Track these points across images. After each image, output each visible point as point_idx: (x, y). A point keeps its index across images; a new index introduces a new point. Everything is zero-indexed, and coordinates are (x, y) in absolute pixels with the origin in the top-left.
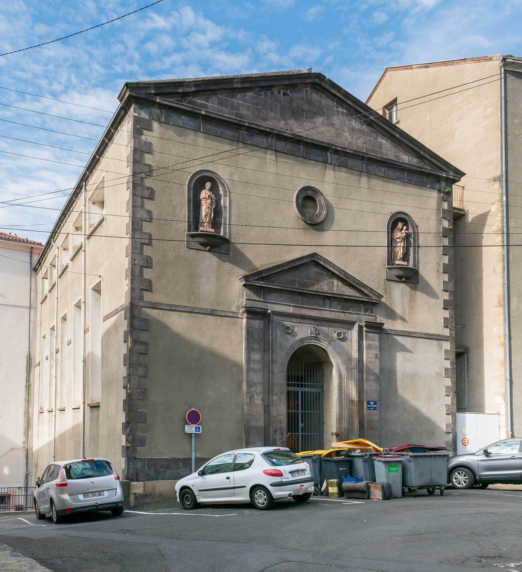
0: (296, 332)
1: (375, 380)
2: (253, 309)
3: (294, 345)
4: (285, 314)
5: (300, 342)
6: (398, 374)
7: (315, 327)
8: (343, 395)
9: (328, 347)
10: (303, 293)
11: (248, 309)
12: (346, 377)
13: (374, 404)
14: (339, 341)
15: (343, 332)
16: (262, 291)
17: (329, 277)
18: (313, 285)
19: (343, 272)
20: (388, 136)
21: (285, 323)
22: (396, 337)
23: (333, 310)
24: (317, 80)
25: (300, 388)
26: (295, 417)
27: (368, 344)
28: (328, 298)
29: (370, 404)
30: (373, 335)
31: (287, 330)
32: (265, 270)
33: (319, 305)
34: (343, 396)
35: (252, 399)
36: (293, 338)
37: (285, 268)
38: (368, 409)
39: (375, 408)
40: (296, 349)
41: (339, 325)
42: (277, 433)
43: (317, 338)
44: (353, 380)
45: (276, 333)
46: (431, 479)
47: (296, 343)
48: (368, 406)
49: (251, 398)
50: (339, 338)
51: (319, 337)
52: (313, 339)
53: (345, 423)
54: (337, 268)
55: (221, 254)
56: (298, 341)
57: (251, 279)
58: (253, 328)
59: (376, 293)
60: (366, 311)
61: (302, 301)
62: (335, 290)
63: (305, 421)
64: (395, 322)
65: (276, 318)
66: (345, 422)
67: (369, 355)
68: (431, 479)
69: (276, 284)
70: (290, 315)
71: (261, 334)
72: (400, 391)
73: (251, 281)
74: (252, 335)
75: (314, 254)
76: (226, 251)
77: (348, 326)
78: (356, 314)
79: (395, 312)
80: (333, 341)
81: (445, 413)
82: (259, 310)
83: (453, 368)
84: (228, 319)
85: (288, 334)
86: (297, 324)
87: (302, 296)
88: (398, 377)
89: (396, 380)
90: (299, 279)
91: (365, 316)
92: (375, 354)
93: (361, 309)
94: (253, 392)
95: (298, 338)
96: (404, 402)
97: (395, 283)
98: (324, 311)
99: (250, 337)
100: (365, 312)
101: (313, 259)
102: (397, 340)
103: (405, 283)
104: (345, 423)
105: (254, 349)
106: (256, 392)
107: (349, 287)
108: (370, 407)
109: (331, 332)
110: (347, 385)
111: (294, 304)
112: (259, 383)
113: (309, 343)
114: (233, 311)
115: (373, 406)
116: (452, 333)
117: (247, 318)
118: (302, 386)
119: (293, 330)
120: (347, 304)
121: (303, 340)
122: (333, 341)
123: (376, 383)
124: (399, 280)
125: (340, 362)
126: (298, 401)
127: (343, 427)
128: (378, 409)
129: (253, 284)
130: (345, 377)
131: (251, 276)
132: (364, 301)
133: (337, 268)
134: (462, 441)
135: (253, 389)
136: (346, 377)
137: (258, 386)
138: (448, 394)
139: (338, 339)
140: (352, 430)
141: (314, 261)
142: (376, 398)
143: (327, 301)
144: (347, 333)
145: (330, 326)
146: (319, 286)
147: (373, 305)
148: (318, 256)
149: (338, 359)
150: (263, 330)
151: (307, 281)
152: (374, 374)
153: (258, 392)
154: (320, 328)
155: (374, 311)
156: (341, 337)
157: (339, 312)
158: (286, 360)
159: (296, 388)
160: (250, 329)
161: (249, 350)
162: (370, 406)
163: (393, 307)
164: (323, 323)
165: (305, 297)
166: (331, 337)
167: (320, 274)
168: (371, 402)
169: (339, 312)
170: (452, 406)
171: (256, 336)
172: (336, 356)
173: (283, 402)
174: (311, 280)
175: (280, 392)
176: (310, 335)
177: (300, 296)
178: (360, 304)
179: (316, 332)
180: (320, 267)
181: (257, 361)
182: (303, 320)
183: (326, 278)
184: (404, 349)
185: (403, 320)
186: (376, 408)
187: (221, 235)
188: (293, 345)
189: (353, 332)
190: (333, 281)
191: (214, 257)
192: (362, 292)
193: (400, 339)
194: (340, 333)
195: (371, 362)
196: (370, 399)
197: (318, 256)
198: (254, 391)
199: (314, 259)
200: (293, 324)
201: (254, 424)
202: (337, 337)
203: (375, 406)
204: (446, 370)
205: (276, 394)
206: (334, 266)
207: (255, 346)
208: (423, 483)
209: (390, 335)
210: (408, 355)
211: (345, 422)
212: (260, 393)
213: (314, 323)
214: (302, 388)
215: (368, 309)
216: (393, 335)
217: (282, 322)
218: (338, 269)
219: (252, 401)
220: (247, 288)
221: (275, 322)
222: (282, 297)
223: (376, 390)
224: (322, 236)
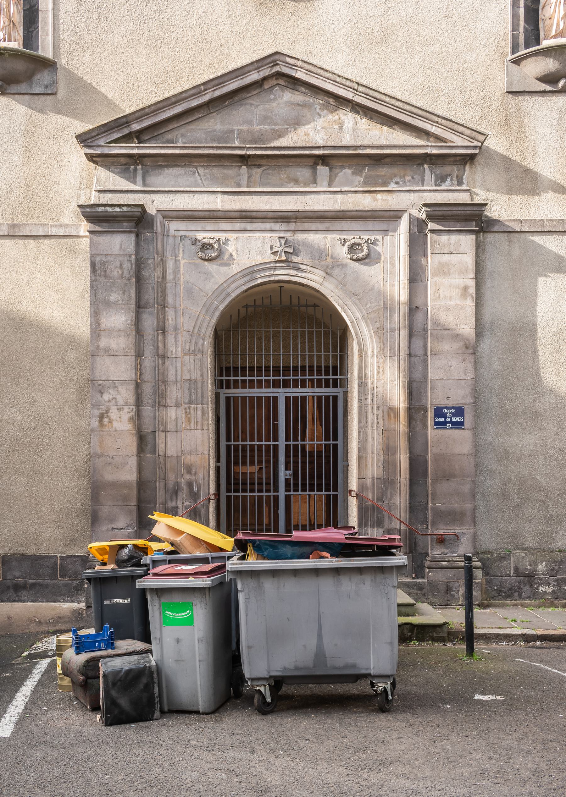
0: (231, 255)
1: (459, 352)
2: (100, 209)
3: (228, 286)
4: (197, 213)
5: (244, 276)
7: (283, 238)
8: (370, 396)
9: (326, 284)
10: (249, 156)
11: (88, 210)
12: (375, 353)
13: (454, 415)
14: (356, 264)
15: (367, 241)
16: (139, 167)
17: (328, 109)
18: (280, 135)
19: (361, 89)
21: (200, 236)
22: (537, 239)
23: (339, 189)
25: (281, 390)
26: (328, 457)
27: (439, 263)
28: (324, 160)
29: (445, 416)
30: (454, 238)
31: (206, 252)
32: (137, 115)
33: (296, 181)
34: (369, 401)
35: (106, 420)
36: (223, 269)
37: (194, 103)
38: (437, 428)
39: (459, 425)
40: (233, 295)
41: (355, 225)
42: (180, 493)
43: (292, 264)
44: (396, 358)
45: (176, 261)
46: (320, 655)
47: (234, 282)
48: (438, 420)
49: (101, 417)
50: (355, 257)
51: (295, 259)
52: (282, 268)
53: (372, 465)
54: (344, 81)
55: (36, 97)
56: (239, 275)
57: (102, 140)
58: (106, 255)
59: (461, 129)
60: (441, 179)
61: (249, 177)
62: (347, 139)
63: (296, 462)
64: (536, 198)
65: (174, 226)
66: (373, 461)
67: (441, 290)
68: (320, 655)
69: (179, 145)
70: (211, 214)
71: (129, 266)
73: (99, 146)
74: (105, 272)
75: (277, 57)
76: (46, 87)
77: (384, 226)
78: (409, 191)
80: (338, 266)
82: (118, 209)
84: (53, 242)
85: (210, 260)
86: (234, 235)
87: (247, 165)
89: (535, 350)
90: (245, 127)
91: (436, 194)
92: (462, 286)
93: (426, 178)
94: (107, 404)
95: (235, 269)
97: (537, 99)
98: (313, 196)
99: (100, 276)
100: (436, 185)
101: (277, 69)
102: (541, 248)
104: (372, 465)
105: (108, 304)
106: (116, 402)
107: (390, 126)
108: (445, 423)
109: (333, 246)
110: (378, 372)
111: (228, 186)
112: (124, 382)
113: (272, 279)
114: (65, 222)
115: (454, 419)
117: (91, 232)
118: (286, 384)
119: (220, 253)
120: (383, 171)
121: (251, 271)
122: (338, 266)
123: (464, 360)
124: (549, 88)
125: (359, 315)
126: (276, 418)
127: (369, 474)
128: (467, 424)
129: (106, 151)
130: (373, 351)
131: (98, 135)
132: (426, 154)
133: (344, 81)
135: (106, 397)
136: (375, 353)
137: (120, 389)
139: (351, 259)
140: (393, 482)
141: (280, 75)
142: (464, 397)
143: (323, 170)
144: (380, 244)
145: (327, 230)
146: (302, 135)
147: (465, 164)
148: (288, 60)
149: (353, 308)
150: (133, 257)
151: (266, 127)
152: (457, 337)
153: (121, 402)
154: (300, 236)
155: (467, 178)
156: (361, 255)
157: (356, 192)
158: (205, 324)
159: (271, 390)
160: (98, 259)
162: (442, 420)
163: (529, 163)
164: (307, 225)
165: (259, 166)
166: (332, 258)
167: (303, 105)
168: (445, 411)
169: (356, 192)
171: (116, 273)
172: (349, 303)
173: (196, 423)
174: (275, 124)
175: (187, 401)
176: (273, 258)
177: (244, 167)
178: (421, 164)
179: (287, 250)
180: (303, 89)
181: (119, 330)
182: (251, 222)
183: (319, 114)
186: (462, 423)
187: (41, 53)
188: (225, 285)
189: (397, 237)
190: (343, 117)
191: (18, 105)
192: (427, 134)
194: (359, 244)
195: (448, 309)
196: (442, 402)
197: (288, 60)
198: (109, 401)
199: (279, 70)
200: (223, 236)
201: (109, 476)
202: (349, 256)
203: (460, 419)
205: (177, 405)
206: (335, 77)
207: (113, 297)
208: (285, 669)
209: (516, 235)
211: (373, 461)
212: (127, 403)
213: (283, 228)
214: (287, 390)
215: (447, 176)
216: (527, 234)
217: (191, 234)
218: (347, 82)
219: (106, 423)
220: (100, 166)
221: (174, 237)
222: (194, 173)
223: (464, 377)
224: (311, 12)
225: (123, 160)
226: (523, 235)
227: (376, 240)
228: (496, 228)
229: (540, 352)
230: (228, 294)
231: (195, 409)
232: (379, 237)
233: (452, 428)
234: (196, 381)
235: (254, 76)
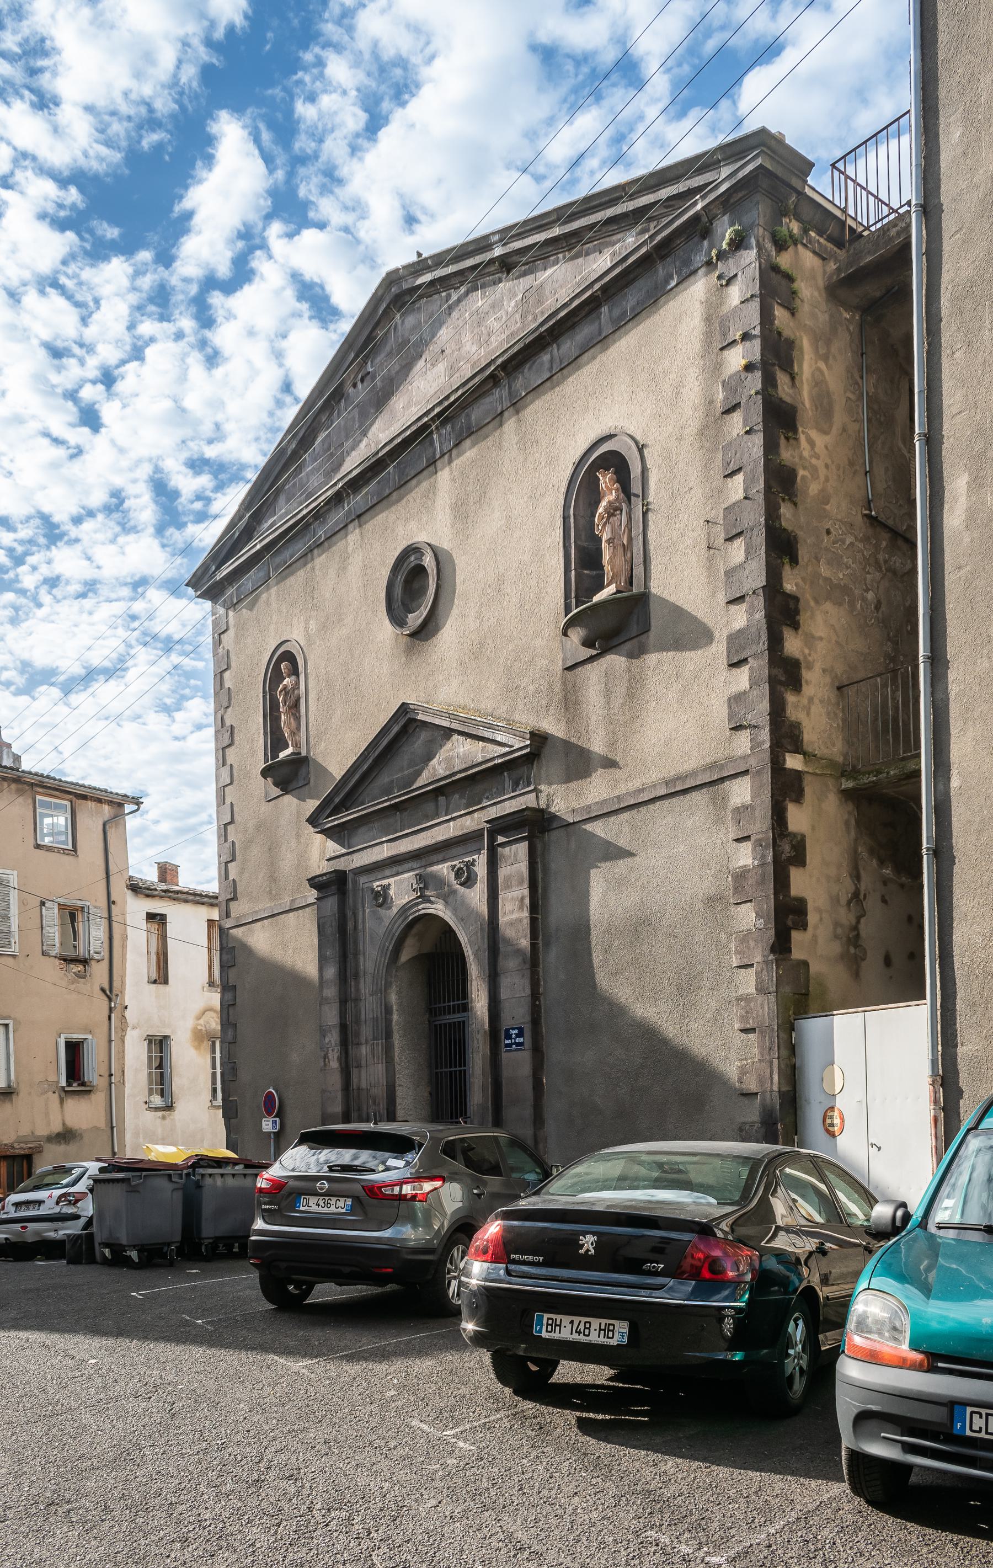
3: (393, 927)
5: (400, 916)
6: (593, 934)
13: (518, 1036)
18: (418, 774)
20: (550, 249)
24: (394, 290)
41: (459, 850)
45: (364, 911)
47: (395, 922)
60: (516, 785)
64: (588, 780)
72: (602, 980)
79: (589, 751)
81: (736, 1026)
83: (762, 865)
88: (594, 942)
96: (616, 1011)
103: (614, 650)
115: (517, 1040)
116: (760, 738)
121: (404, 909)
134: (824, 1120)
138: (746, 961)
143: (442, 799)
161: (322, 960)
165: (405, 809)
170: (759, 1001)
184: (614, 853)
185: (610, 764)
193: (597, 828)
200: (385, 882)
203: (521, 1040)
204: (740, 877)
210: (621, 866)
225: (337, 829)
226: (577, 826)
227: (474, 860)
228: (555, 825)
229: (594, 955)
230: (394, 935)
231: (378, 1044)
232: (475, 857)
233: (516, 1050)
234: (377, 1018)
235: (396, 729)
